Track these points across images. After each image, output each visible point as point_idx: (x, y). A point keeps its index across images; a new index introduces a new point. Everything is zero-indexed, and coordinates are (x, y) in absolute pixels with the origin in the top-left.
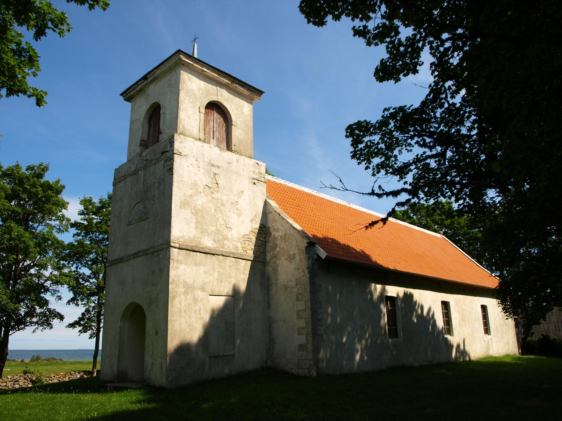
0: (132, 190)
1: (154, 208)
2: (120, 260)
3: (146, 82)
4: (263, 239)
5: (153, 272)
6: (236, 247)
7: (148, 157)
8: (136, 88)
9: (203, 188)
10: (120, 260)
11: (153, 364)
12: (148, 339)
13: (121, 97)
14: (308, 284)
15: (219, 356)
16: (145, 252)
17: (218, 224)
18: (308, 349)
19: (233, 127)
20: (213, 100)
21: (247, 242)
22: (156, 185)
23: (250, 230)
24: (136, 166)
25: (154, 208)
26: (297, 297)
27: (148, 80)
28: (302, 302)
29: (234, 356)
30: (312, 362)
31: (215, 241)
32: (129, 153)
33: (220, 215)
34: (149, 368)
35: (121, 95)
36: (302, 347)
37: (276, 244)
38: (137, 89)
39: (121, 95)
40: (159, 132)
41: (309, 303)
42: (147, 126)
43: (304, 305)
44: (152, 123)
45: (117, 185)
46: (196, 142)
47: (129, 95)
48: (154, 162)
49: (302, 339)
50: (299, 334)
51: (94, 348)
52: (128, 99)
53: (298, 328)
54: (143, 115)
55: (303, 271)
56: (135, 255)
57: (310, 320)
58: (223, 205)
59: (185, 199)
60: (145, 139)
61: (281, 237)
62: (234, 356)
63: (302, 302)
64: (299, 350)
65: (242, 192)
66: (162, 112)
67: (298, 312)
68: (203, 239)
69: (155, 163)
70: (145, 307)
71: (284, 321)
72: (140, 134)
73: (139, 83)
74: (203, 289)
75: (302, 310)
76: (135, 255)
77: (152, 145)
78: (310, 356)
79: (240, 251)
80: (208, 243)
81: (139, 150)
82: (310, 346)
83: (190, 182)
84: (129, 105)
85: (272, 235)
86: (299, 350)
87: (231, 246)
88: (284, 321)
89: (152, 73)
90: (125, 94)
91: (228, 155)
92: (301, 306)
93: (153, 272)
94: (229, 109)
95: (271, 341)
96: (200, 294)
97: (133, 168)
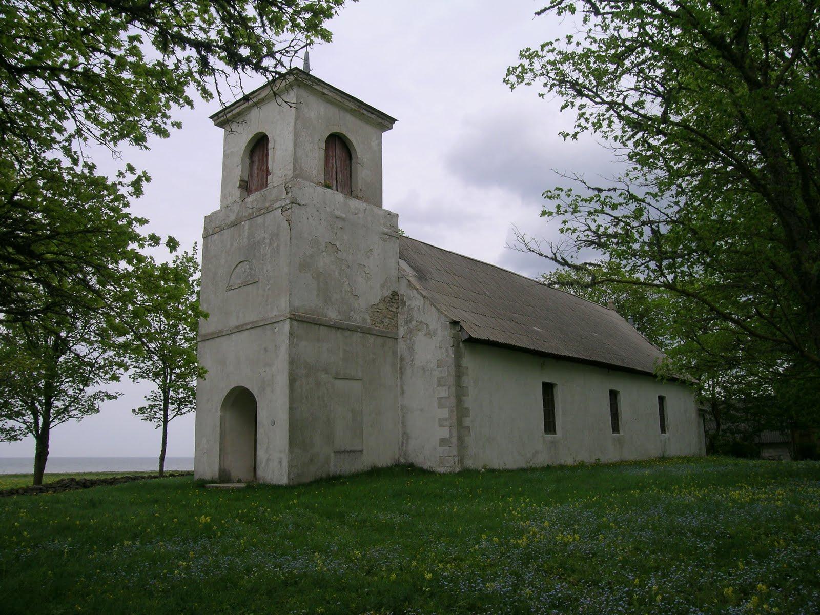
0: (232, 245)
1: (265, 271)
2: (219, 335)
3: (246, 105)
4: (395, 310)
5: (266, 350)
6: (364, 320)
7: (255, 204)
8: (232, 110)
9: (325, 245)
10: (219, 335)
11: (268, 460)
12: (260, 431)
13: (211, 122)
14: (453, 366)
15: (345, 452)
16: (254, 326)
17: (344, 291)
18: (451, 443)
19: (359, 167)
20: (335, 131)
21: (376, 314)
22: (267, 241)
23: (379, 298)
24: (238, 214)
25: (265, 271)
26: (439, 382)
27: (251, 102)
28: (446, 388)
29: (361, 451)
30: (456, 459)
31: (339, 313)
32: (224, 197)
33: (345, 279)
34: (263, 465)
35: (211, 118)
36: (443, 442)
37: (412, 317)
38: (234, 112)
39: (211, 118)
40: (268, 173)
41: (453, 389)
42: (248, 161)
43: (447, 393)
44: (256, 159)
45: (209, 238)
46: (317, 188)
47: (222, 119)
48: (263, 211)
49: (444, 433)
50: (441, 426)
51: (32, 470)
52: (220, 125)
53: (440, 419)
54: (244, 148)
55: (447, 351)
56: (240, 329)
57: (454, 409)
58: (349, 267)
59: (304, 260)
60: (246, 179)
61: (419, 308)
62: (361, 451)
63: (446, 388)
64: (441, 446)
65: (371, 250)
66: (270, 145)
67: (440, 399)
68: (326, 310)
69: (264, 214)
70: (255, 393)
71: (422, 410)
72: (238, 173)
73: (236, 105)
74: (326, 371)
75: (446, 398)
76: (240, 329)
77: (257, 190)
78: (455, 453)
79: (368, 325)
80: (333, 315)
81: (237, 192)
82: (454, 440)
83: (310, 239)
84: (221, 131)
85: (407, 304)
86: (441, 446)
87: (358, 318)
88: (422, 410)
89: (256, 94)
90: (216, 118)
91: (354, 203)
92: (444, 392)
93: (266, 350)
94: (354, 143)
95: (406, 436)
96: (323, 377)
97: (232, 217)
